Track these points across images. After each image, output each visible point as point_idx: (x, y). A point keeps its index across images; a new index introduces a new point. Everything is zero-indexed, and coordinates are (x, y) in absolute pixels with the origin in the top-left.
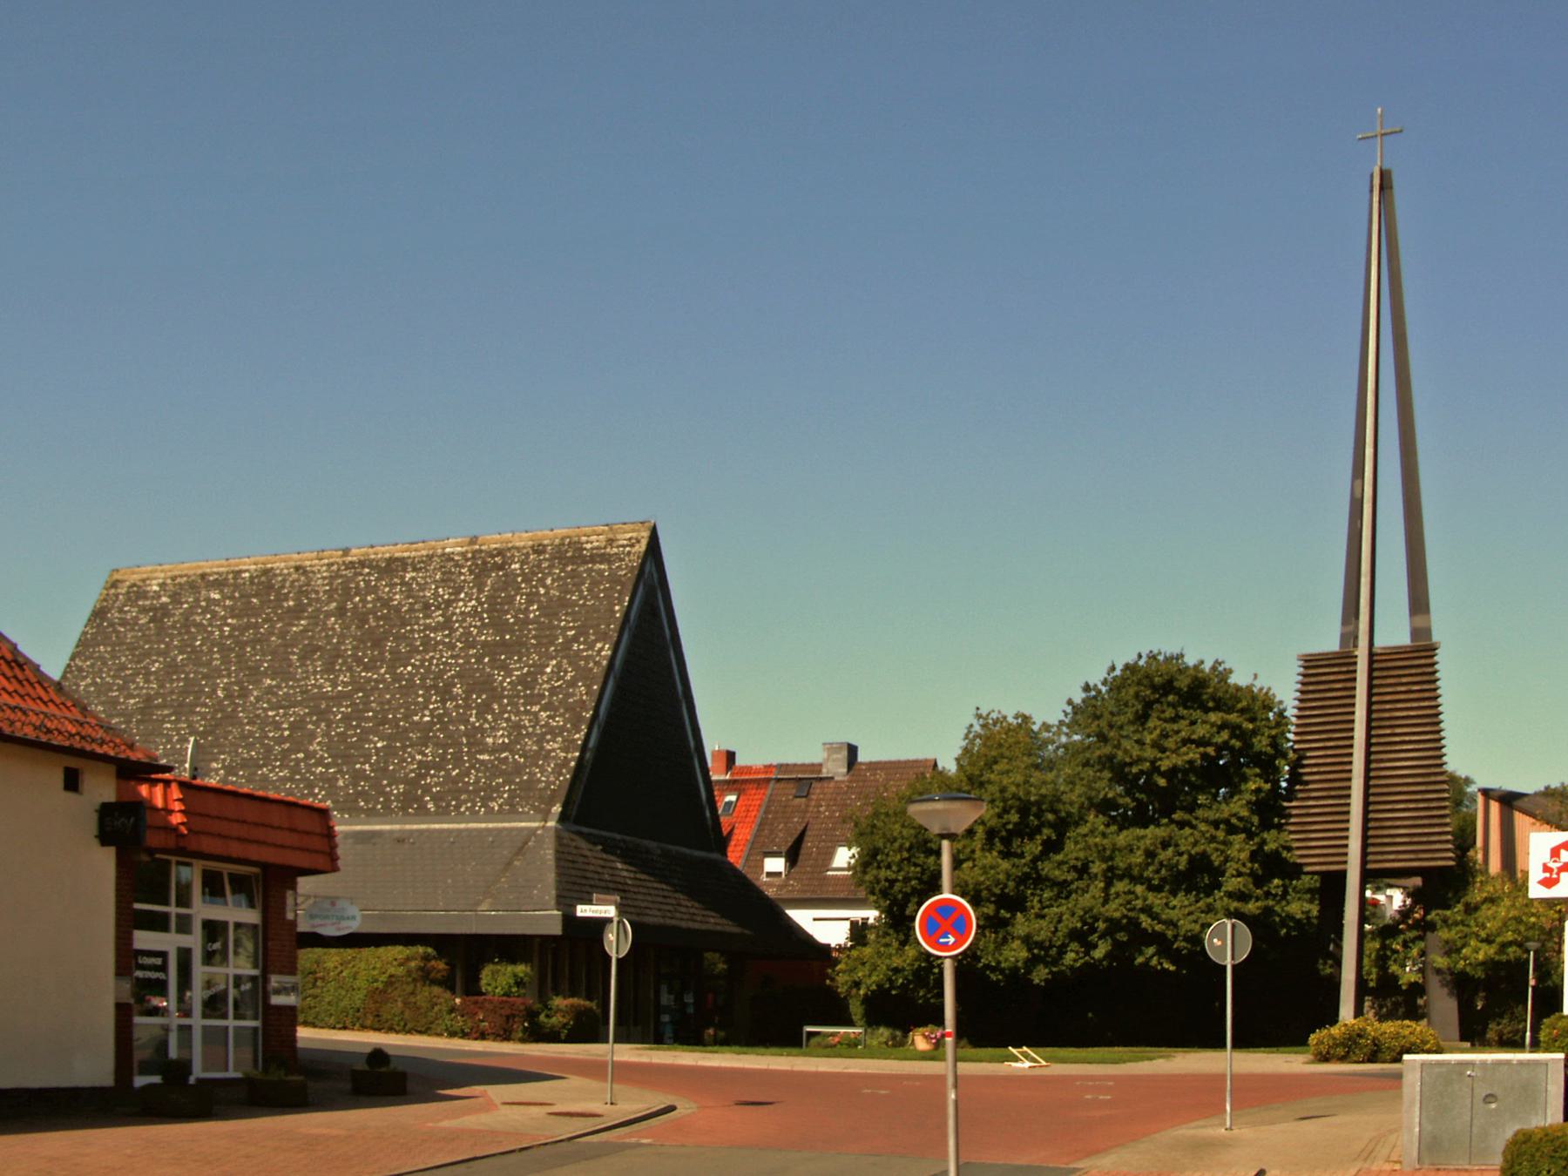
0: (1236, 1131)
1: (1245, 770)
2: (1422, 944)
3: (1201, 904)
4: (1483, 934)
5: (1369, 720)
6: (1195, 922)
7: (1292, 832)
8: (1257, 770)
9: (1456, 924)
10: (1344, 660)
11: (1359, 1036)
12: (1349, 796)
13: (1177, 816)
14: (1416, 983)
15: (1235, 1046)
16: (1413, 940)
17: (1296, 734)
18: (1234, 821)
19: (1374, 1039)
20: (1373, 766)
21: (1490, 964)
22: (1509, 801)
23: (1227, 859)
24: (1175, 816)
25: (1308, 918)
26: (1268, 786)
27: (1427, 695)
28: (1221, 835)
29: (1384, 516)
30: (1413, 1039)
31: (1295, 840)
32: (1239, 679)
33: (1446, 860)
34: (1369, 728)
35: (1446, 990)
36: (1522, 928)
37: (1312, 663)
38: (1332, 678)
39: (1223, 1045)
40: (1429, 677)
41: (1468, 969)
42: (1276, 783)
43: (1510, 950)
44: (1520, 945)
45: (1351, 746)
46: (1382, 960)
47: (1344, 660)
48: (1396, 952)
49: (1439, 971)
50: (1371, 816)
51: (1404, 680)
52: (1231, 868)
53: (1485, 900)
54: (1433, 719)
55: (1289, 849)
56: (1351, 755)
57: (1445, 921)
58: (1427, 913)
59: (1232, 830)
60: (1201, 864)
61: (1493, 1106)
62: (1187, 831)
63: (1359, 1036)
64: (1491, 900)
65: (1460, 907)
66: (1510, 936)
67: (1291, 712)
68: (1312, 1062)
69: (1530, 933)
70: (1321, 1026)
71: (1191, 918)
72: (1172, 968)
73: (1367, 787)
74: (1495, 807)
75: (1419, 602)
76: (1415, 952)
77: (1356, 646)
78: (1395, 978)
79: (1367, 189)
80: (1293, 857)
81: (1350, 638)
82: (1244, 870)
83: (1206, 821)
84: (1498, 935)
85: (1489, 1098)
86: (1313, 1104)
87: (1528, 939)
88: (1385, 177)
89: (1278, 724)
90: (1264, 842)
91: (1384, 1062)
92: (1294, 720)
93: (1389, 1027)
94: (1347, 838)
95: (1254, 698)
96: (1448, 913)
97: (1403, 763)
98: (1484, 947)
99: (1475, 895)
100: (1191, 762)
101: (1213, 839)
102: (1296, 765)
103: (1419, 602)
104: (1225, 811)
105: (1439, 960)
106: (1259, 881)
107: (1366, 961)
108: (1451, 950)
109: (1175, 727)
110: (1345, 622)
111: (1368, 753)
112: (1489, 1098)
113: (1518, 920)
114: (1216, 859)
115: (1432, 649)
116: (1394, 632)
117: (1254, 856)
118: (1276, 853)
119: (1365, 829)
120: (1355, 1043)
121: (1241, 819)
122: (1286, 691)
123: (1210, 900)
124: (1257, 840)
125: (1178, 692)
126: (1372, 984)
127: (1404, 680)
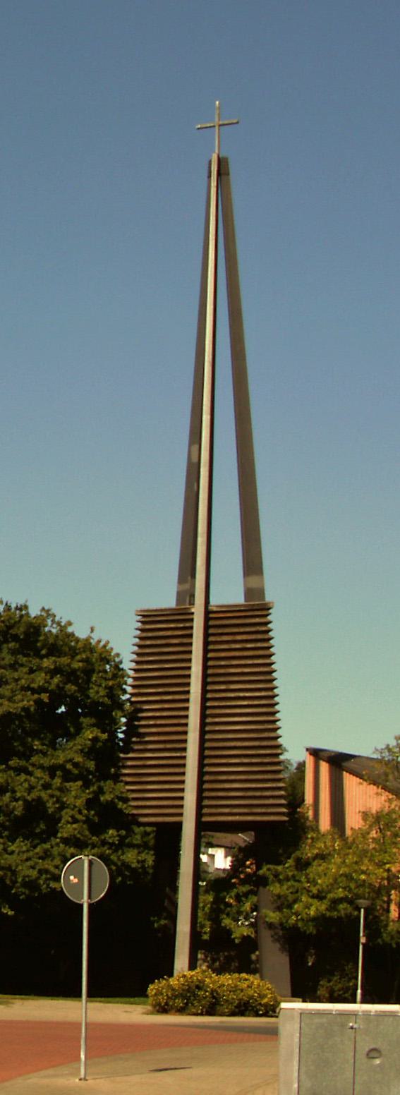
0: (90, 1082)
1: (82, 719)
2: (255, 899)
3: (38, 850)
4: (314, 890)
5: (205, 675)
6: (33, 868)
7: (127, 783)
8: (93, 721)
9: (287, 879)
10: (180, 616)
11: (198, 987)
12: (185, 749)
13: (14, 762)
14: (249, 937)
15: (90, 995)
16: (246, 895)
17: (134, 687)
18: (69, 766)
19: (212, 991)
20: (209, 720)
21: (320, 920)
22: (339, 762)
23: (63, 806)
24: (11, 763)
25: (143, 867)
26: (105, 736)
27: (261, 653)
28: (57, 782)
29: (224, 471)
30: (251, 992)
31: (134, 792)
32: (81, 632)
33: (279, 815)
34: (205, 684)
35: (278, 945)
36: (352, 885)
37: (150, 619)
38: (169, 633)
39: (78, 995)
40: (262, 636)
41: (300, 924)
42: (113, 735)
43: (341, 906)
44: (351, 902)
45: (187, 701)
46: (215, 915)
47: (180, 616)
48: (230, 905)
49: (271, 926)
50: (207, 769)
51: (239, 638)
52: (66, 815)
53: (316, 857)
54: (266, 677)
55: (125, 800)
56: (187, 709)
57: (276, 875)
58: (259, 868)
59: (68, 777)
60: (35, 810)
61: (378, 1062)
62: (23, 777)
63: (198, 987)
64: (322, 857)
65: (290, 862)
66: (340, 893)
67: (128, 665)
68: (152, 1013)
69: (361, 891)
70: (160, 977)
71: (28, 863)
72: (11, 913)
73: (202, 740)
74: (324, 767)
75: (252, 564)
76: (247, 906)
77: (192, 603)
78: (229, 932)
79: (206, 175)
80: (129, 809)
81: (186, 596)
82: (79, 817)
83: (42, 767)
84: (330, 892)
85: (373, 1053)
86: (164, 1056)
87: (358, 896)
88: (222, 163)
89: (115, 676)
90: (101, 791)
91: (222, 1015)
92: (131, 673)
93: (227, 979)
94: (183, 790)
95: (92, 650)
96: (280, 868)
97: (237, 720)
98: (315, 901)
99: (308, 851)
100: (25, 709)
101: (46, 786)
102: (133, 717)
103: (252, 564)
104: (61, 757)
105: (272, 914)
106: (96, 829)
107: (200, 914)
108: (283, 904)
109: (16, 675)
110: (181, 580)
111: (204, 708)
112: (373, 1053)
113: (348, 877)
114: (51, 806)
115: (265, 609)
116: (228, 591)
117: (90, 804)
118: (111, 804)
119: (201, 782)
120: (195, 995)
121: (76, 765)
122: (123, 645)
123: (47, 846)
124: (94, 788)
125: (15, 638)
126: (206, 937)
127: (239, 638)
